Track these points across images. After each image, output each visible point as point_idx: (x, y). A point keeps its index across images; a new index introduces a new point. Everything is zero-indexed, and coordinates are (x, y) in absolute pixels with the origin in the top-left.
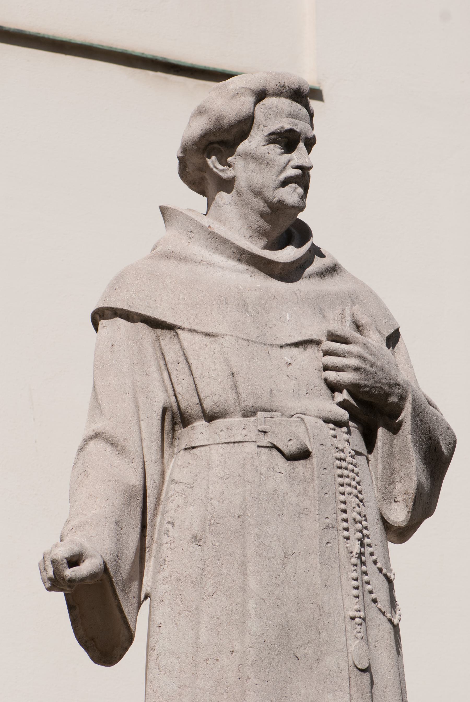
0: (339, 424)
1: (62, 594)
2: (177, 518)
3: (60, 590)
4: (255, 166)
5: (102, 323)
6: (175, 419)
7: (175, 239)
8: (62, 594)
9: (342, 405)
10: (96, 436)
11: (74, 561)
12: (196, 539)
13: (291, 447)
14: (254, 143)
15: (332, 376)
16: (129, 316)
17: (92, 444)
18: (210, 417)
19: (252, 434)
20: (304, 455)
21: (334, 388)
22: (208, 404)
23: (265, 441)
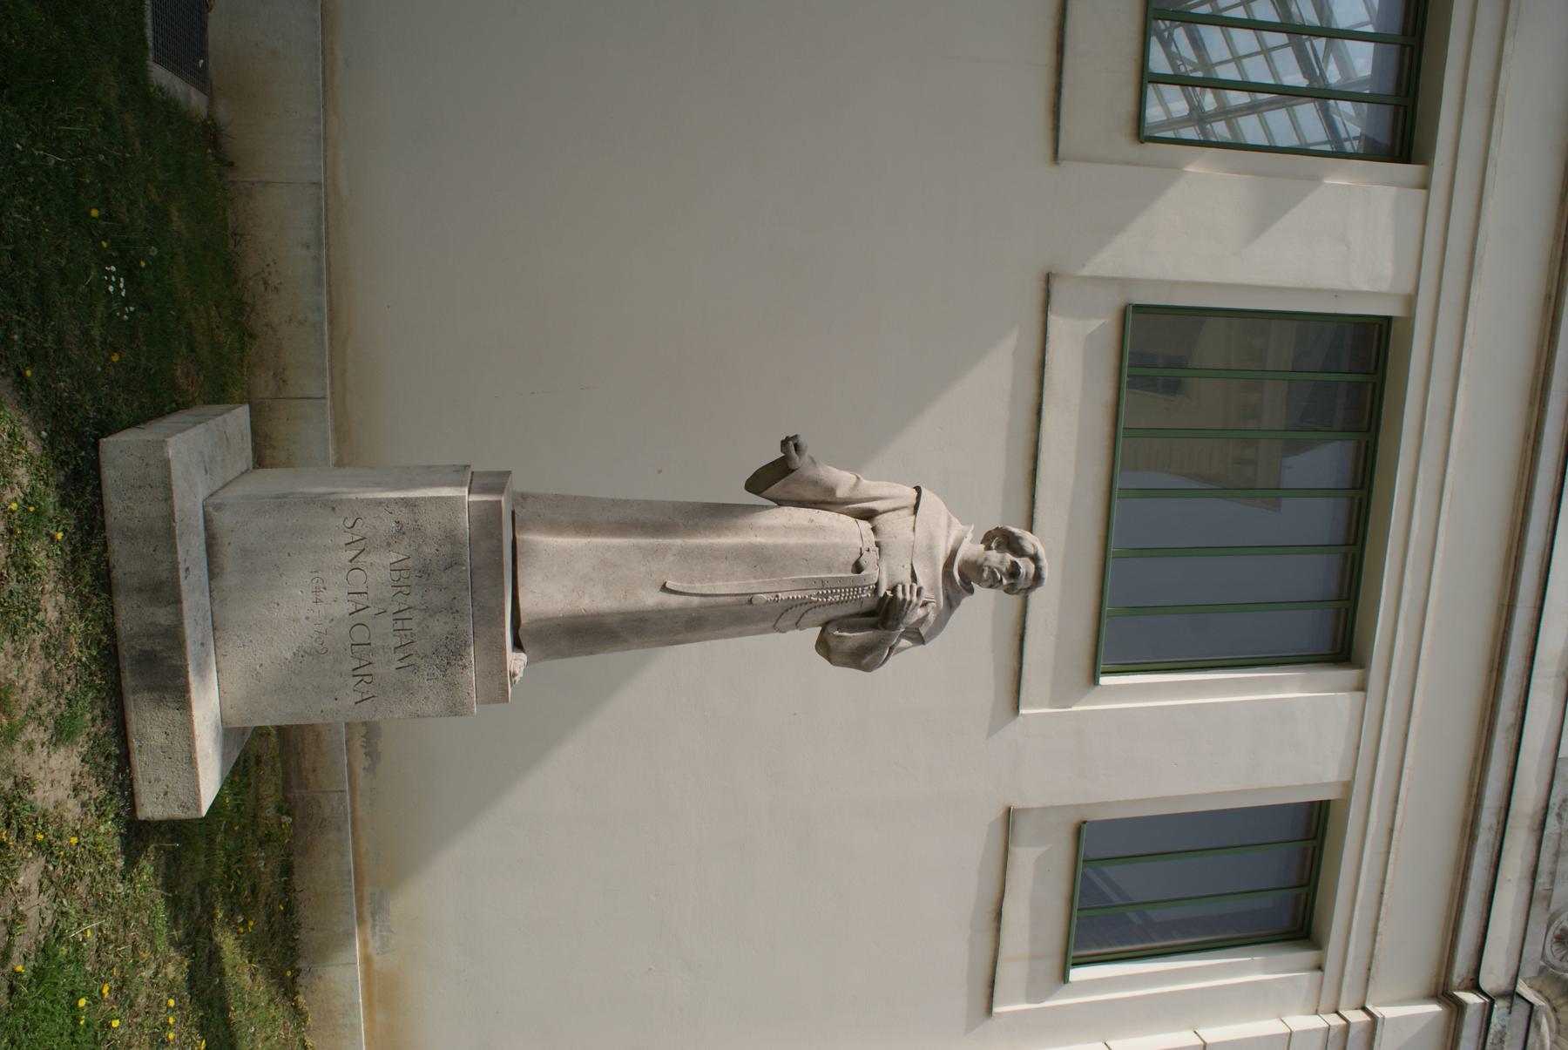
11: (797, 447)
20: (858, 568)
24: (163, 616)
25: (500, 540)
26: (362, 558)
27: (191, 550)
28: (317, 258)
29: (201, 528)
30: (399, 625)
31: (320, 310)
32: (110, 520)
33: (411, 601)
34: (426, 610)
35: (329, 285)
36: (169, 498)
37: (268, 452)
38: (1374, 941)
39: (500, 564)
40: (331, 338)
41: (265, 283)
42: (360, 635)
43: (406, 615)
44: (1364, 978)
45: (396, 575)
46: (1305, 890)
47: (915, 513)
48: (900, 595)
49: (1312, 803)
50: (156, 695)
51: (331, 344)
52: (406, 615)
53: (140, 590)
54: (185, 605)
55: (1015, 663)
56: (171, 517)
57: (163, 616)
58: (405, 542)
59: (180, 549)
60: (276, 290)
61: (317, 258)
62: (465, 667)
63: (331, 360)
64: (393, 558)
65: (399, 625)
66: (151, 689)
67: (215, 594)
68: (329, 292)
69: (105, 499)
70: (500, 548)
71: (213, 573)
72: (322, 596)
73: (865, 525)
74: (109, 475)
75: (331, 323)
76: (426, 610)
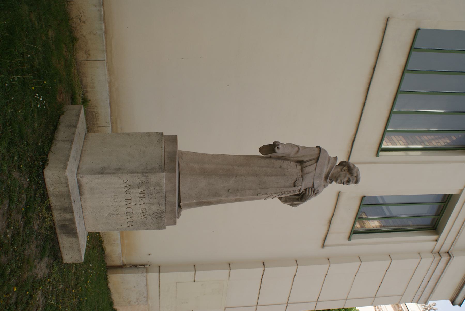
0: (299, 191)
1: (65, 262)
2: (285, 164)
3: (67, 264)
4: (345, 175)
5: (381, 153)
6: (301, 162)
7: (332, 161)
8: (65, 262)
9: (303, 192)
10: (299, 149)
12: (281, 166)
13: (296, 184)
14: (348, 176)
15: (308, 190)
16: (319, 154)
17: (297, 148)
18: (302, 169)
19: (298, 177)
21: (306, 190)
22: (304, 169)
23: (297, 179)
24: (68, 216)
25: (175, 184)
26: (129, 190)
27: (75, 192)
28: (99, 11)
29: (77, 182)
30: (142, 207)
31: (101, 29)
32: (49, 192)
33: (145, 201)
34: (151, 204)
35: (104, 19)
36: (68, 186)
37: (84, 79)
38: (457, 235)
39: (175, 190)
40: (106, 39)
41: (80, 19)
42: (129, 210)
43: (144, 205)
44: (451, 244)
45: (141, 195)
46: (437, 217)
47: (317, 162)
48: (307, 192)
49: (445, 195)
50: (67, 235)
51: (106, 40)
52: (144, 205)
53: (60, 210)
54: (75, 213)
55: (350, 150)
56: (69, 191)
57: (68, 216)
58: (144, 186)
59: (72, 199)
60: (85, 22)
61: (99, 11)
62: (162, 218)
63: (106, 47)
64: (140, 190)
65: (142, 207)
66: (65, 233)
67: (82, 199)
68: (105, 22)
69: (47, 187)
70: (175, 186)
71: (81, 193)
72: (116, 200)
73: (299, 167)
74: (48, 180)
75: (106, 33)
76: (151, 204)
